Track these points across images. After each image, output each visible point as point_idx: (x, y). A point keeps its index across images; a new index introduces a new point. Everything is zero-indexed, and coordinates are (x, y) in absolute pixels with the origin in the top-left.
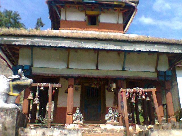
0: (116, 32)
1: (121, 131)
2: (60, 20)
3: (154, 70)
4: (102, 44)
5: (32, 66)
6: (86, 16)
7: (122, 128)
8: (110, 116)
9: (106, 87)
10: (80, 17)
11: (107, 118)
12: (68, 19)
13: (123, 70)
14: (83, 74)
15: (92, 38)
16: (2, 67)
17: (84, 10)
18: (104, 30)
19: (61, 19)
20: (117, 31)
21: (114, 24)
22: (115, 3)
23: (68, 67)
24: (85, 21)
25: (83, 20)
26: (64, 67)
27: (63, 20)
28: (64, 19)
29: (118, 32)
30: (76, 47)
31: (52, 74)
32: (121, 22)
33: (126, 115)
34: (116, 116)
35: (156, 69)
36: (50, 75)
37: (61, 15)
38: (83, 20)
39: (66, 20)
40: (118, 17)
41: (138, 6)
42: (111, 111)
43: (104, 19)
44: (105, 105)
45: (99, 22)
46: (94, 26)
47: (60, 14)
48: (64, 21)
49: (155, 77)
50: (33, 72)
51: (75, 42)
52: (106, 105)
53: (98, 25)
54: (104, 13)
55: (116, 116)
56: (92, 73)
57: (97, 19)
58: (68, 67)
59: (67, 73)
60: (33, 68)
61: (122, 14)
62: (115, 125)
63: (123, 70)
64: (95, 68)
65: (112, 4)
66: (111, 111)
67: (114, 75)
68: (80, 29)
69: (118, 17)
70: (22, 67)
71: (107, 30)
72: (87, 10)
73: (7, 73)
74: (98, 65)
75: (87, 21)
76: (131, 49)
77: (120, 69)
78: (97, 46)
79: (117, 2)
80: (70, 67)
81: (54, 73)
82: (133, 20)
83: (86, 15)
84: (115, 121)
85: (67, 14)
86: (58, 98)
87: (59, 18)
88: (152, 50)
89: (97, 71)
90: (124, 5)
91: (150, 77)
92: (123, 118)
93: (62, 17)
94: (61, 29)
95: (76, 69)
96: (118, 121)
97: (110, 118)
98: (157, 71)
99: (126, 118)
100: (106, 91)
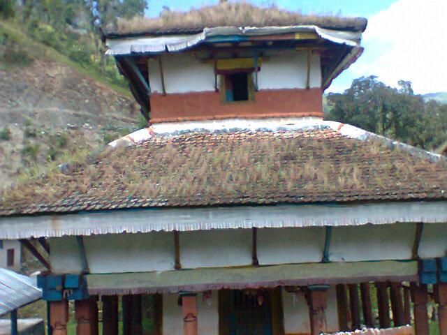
0: (303, 116)
2: (149, 94)
3: (407, 255)
4: (262, 214)
5: (86, 272)
6: (218, 76)
10: (201, 82)
12: (169, 91)
13: (325, 260)
14: (220, 282)
15: (232, 288)
16: (33, 92)
19: (152, 92)
20: (306, 114)
21: (296, 91)
22: (297, 37)
23: (178, 267)
24: (217, 91)
25: (212, 89)
26: (168, 266)
27: (156, 93)
28: (160, 91)
29: (310, 116)
30: (192, 230)
31: (140, 289)
35: (415, 250)
36: (133, 293)
37: (150, 84)
38: (212, 89)
39: (165, 94)
40: (309, 72)
43: (269, 79)
47: (148, 82)
48: (159, 95)
49: (411, 274)
50: (89, 288)
51: (188, 216)
52: (283, 327)
53: (253, 99)
54: (267, 59)
56: (243, 277)
57: (249, 81)
58: (178, 267)
59: (178, 282)
60: (88, 277)
61: (319, 59)
63: (325, 260)
64: (249, 261)
65: (290, 41)
67: (300, 278)
68: (205, 117)
69: (309, 72)
71: (278, 114)
72: (221, 59)
73: (47, 107)
74: (256, 254)
75: (223, 91)
76: (344, 222)
77: (317, 258)
78: (250, 223)
80: (185, 264)
81: (144, 285)
83: (217, 72)
85: (164, 75)
86: (162, 319)
87: (146, 91)
88: (404, 218)
89: (256, 270)
91: (399, 275)
93: (154, 87)
95: (197, 269)
98: (415, 258)
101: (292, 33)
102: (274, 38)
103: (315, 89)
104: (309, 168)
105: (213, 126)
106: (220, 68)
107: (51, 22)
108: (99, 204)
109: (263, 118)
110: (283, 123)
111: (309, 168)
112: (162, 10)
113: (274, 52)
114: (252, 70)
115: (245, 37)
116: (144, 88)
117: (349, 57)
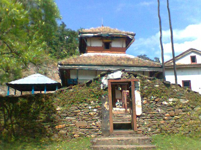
1: (123, 111)
5: (77, 79)
7: (124, 109)
8: (118, 103)
9: (116, 87)
10: (99, 44)
11: (116, 105)
17: (102, 39)
18: (114, 52)
21: (120, 48)
22: (121, 36)
32: (124, 46)
33: (126, 103)
34: (121, 104)
37: (87, 41)
39: (91, 46)
41: (135, 37)
42: (118, 101)
43: (114, 45)
44: (115, 97)
45: (111, 47)
46: (108, 50)
47: (86, 41)
54: (114, 40)
55: (121, 104)
60: (78, 81)
62: (121, 108)
66: (118, 101)
70: (12, 27)
71: (116, 52)
79: (121, 114)
82: (133, 46)
84: (121, 106)
90: (126, 37)
92: (125, 105)
93: (88, 44)
94: (88, 52)
96: (122, 106)
97: (118, 105)
99: (126, 105)
100: (116, 90)
101: (120, 35)
102: (116, 36)
103: (124, 48)
104: (123, 61)
105: (101, 54)
106: (104, 41)
107: (55, 128)
108: (10, 48)
109: (113, 53)
110: (117, 54)
111: (123, 61)
112: (80, 28)
113: (115, 39)
114: (111, 42)
115: (110, 35)
116: (85, 42)
117: (132, 41)
